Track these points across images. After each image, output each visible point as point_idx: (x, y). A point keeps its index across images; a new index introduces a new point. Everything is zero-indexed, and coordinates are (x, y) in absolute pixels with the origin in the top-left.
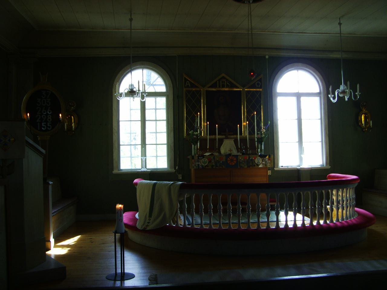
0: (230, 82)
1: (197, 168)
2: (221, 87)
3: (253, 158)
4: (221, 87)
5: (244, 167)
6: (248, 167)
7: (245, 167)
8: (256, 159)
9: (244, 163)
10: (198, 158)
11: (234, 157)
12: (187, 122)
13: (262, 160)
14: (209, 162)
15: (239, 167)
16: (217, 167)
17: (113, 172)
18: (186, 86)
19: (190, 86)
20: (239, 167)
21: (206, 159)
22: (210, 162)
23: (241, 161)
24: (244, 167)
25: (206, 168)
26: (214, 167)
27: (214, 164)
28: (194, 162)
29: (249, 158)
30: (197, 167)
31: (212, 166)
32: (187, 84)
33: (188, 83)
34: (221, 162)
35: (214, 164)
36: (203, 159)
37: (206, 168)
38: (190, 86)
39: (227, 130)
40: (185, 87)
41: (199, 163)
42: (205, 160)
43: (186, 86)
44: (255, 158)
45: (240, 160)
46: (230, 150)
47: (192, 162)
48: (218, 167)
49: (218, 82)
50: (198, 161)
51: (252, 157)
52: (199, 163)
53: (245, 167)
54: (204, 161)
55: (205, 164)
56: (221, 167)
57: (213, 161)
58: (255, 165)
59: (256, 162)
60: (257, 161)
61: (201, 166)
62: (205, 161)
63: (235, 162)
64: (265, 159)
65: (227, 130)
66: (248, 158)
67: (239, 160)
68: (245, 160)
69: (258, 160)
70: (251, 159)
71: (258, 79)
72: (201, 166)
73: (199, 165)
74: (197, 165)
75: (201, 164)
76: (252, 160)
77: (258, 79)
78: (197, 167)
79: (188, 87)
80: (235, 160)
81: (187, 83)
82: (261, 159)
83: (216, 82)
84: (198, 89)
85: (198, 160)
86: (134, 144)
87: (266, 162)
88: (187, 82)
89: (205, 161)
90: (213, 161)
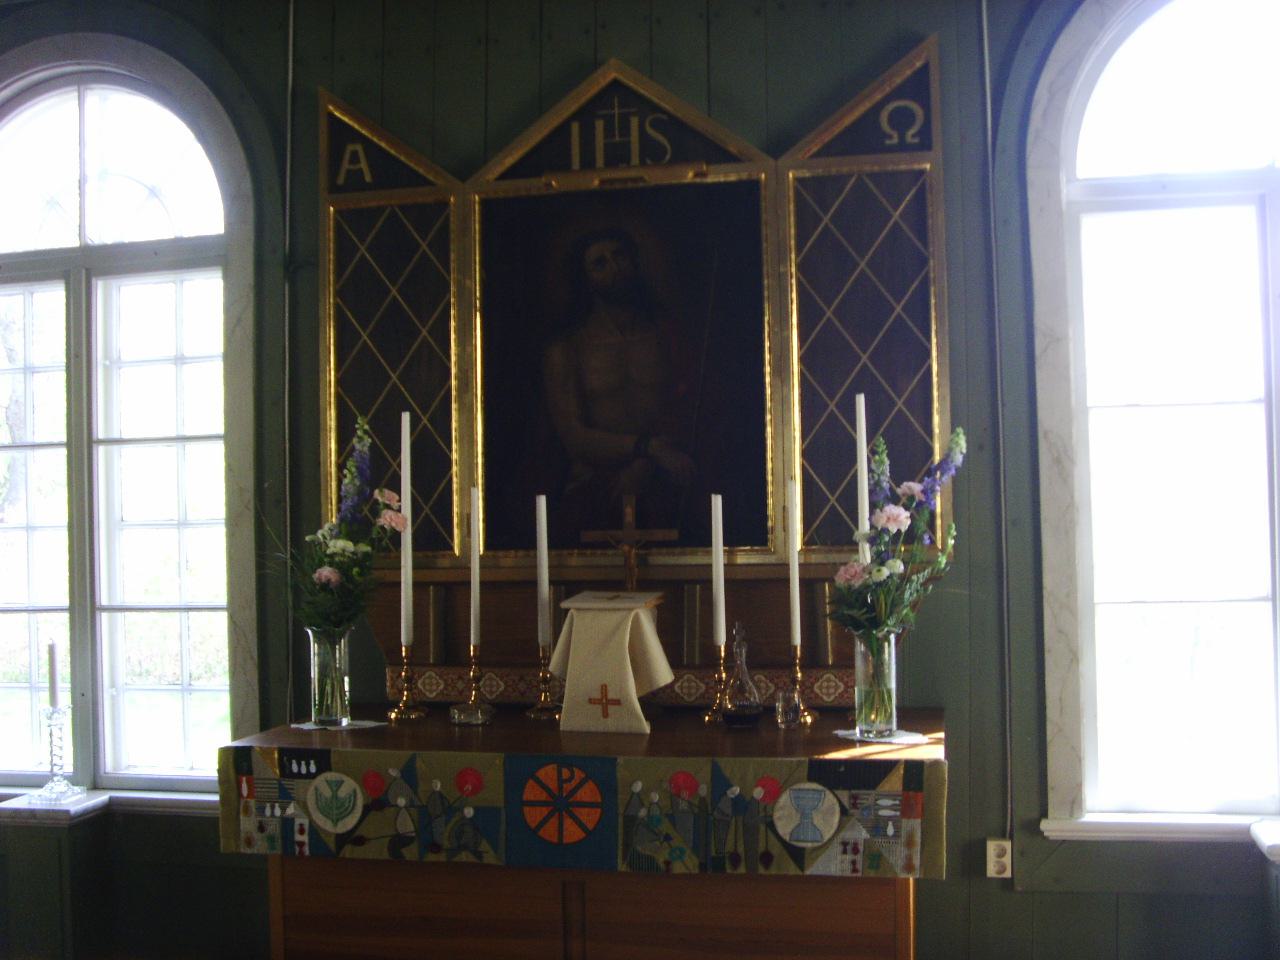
0: (673, 126)
1: (279, 851)
2: (600, 162)
3: (758, 793)
4: (600, 162)
5: (668, 863)
6: (703, 867)
7: (678, 868)
8: (785, 799)
9: (665, 827)
10: (286, 772)
11: (579, 774)
12: (446, 387)
13: (844, 812)
14: (367, 810)
15: (622, 867)
16: (431, 857)
17: (1044, 825)
18: (341, 180)
19: (368, 178)
20: (622, 867)
21: (349, 785)
22: (377, 804)
23: (643, 813)
24: (668, 863)
25: (349, 852)
26: (410, 853)
27: (407, 825)
28: (252, 803)
29: (720, 783)
30: (271, 839)
31: (398, 841)
32: (346, 165)
33: (355, 158)
34: (469, 812)
35: (407, 825)
36: (320, 780)
37: (349, 852)
38: (368, 178)
39: (629, 513)
40: (334, 188)
41: (291, 810)
42: (340, 783)
43: (341, 180)
44: (773, 794)
45: (640, 799)
46: (611, 695)
47: (240, 795)
48: (442, 857)
49: (575, 127)
50: (285, 797)
51: (745, 775)
52: (291, 810)
53: (678, 868)
54: (327, 793)
55: (335, 822)
56: (465, 857)
57: (402, 802)
58: (776, 849)
59: (784, 828)
60: (796, 820)
61: (305, 838)
62: (343, 792)
63: (591, 818)
64: (867, 797)
65: (629, 513)
66: (703, 790)
67: (622, 799)
68: (683, 805)
69: (804, 814)
70: (740, 797)
71: (903, 73)
72: (305, 838)
73: (287, 823)
74: (274, 828)
75: (309, 816)
76: (742, 804)
77: (898, 80)
78: (279, 844)
79: (355, 182)
80: (532, 804)
81: (347, 156)
82: (830, 798)
83: (563, 130)
84: (421, 196)
85: (286, 782)
86: (191, 446)
87: (877, 827)
88: (350, 148)
89: (343, 792)
90: (402, 802)
